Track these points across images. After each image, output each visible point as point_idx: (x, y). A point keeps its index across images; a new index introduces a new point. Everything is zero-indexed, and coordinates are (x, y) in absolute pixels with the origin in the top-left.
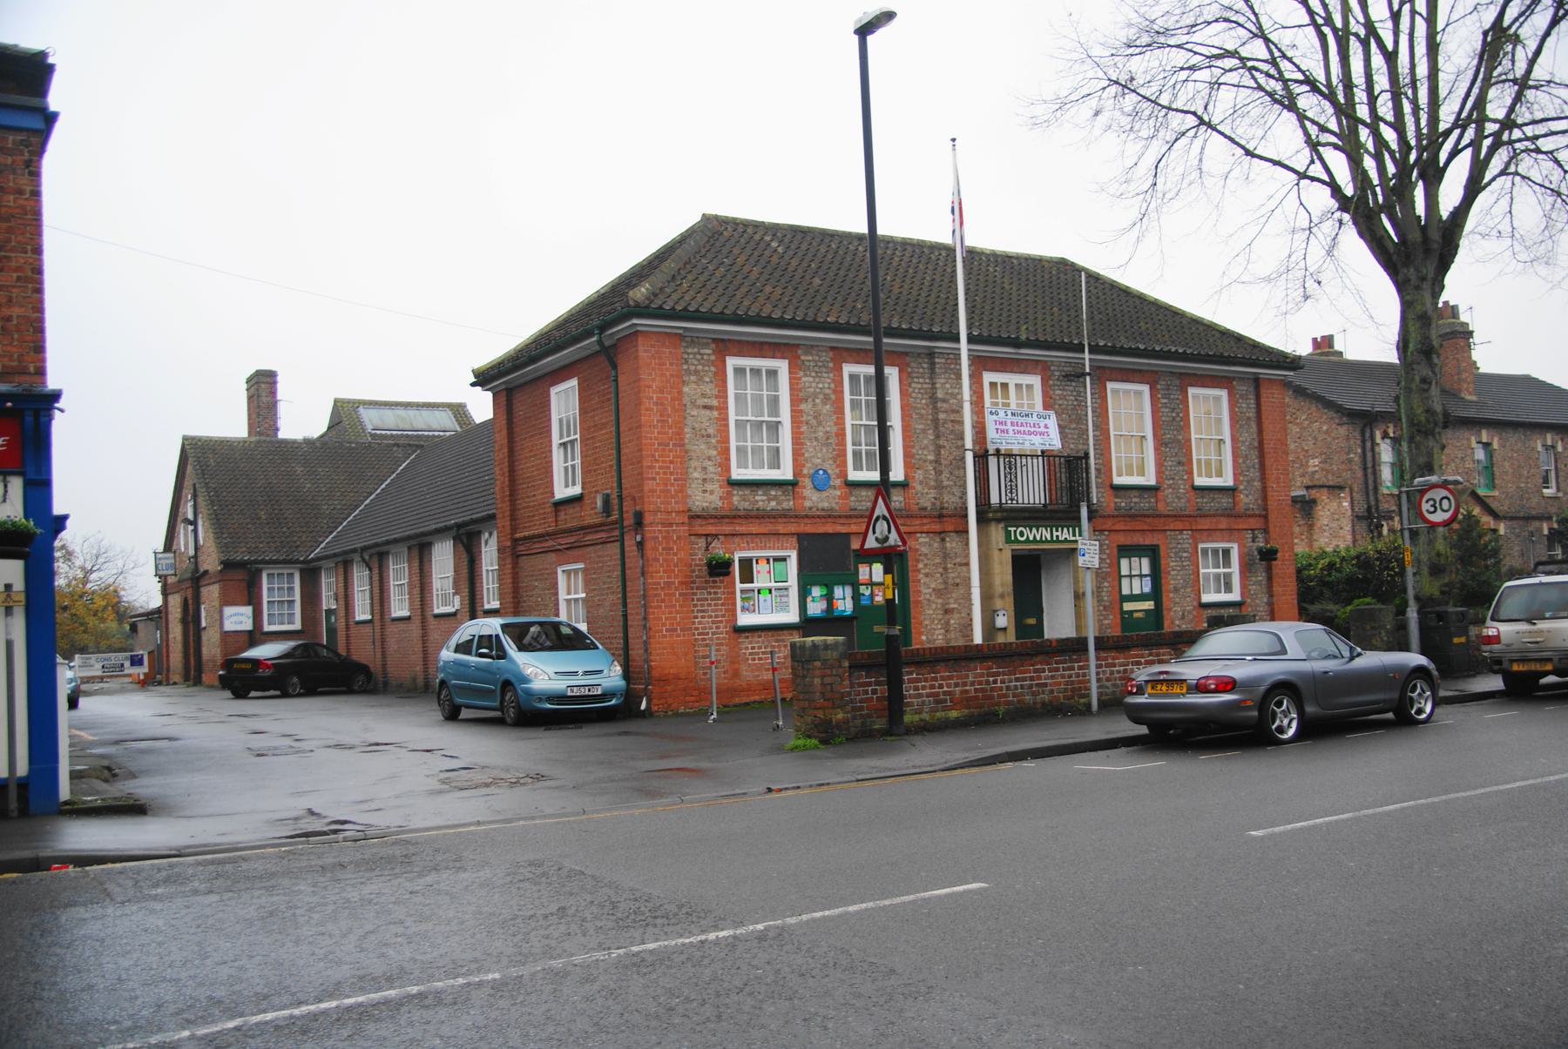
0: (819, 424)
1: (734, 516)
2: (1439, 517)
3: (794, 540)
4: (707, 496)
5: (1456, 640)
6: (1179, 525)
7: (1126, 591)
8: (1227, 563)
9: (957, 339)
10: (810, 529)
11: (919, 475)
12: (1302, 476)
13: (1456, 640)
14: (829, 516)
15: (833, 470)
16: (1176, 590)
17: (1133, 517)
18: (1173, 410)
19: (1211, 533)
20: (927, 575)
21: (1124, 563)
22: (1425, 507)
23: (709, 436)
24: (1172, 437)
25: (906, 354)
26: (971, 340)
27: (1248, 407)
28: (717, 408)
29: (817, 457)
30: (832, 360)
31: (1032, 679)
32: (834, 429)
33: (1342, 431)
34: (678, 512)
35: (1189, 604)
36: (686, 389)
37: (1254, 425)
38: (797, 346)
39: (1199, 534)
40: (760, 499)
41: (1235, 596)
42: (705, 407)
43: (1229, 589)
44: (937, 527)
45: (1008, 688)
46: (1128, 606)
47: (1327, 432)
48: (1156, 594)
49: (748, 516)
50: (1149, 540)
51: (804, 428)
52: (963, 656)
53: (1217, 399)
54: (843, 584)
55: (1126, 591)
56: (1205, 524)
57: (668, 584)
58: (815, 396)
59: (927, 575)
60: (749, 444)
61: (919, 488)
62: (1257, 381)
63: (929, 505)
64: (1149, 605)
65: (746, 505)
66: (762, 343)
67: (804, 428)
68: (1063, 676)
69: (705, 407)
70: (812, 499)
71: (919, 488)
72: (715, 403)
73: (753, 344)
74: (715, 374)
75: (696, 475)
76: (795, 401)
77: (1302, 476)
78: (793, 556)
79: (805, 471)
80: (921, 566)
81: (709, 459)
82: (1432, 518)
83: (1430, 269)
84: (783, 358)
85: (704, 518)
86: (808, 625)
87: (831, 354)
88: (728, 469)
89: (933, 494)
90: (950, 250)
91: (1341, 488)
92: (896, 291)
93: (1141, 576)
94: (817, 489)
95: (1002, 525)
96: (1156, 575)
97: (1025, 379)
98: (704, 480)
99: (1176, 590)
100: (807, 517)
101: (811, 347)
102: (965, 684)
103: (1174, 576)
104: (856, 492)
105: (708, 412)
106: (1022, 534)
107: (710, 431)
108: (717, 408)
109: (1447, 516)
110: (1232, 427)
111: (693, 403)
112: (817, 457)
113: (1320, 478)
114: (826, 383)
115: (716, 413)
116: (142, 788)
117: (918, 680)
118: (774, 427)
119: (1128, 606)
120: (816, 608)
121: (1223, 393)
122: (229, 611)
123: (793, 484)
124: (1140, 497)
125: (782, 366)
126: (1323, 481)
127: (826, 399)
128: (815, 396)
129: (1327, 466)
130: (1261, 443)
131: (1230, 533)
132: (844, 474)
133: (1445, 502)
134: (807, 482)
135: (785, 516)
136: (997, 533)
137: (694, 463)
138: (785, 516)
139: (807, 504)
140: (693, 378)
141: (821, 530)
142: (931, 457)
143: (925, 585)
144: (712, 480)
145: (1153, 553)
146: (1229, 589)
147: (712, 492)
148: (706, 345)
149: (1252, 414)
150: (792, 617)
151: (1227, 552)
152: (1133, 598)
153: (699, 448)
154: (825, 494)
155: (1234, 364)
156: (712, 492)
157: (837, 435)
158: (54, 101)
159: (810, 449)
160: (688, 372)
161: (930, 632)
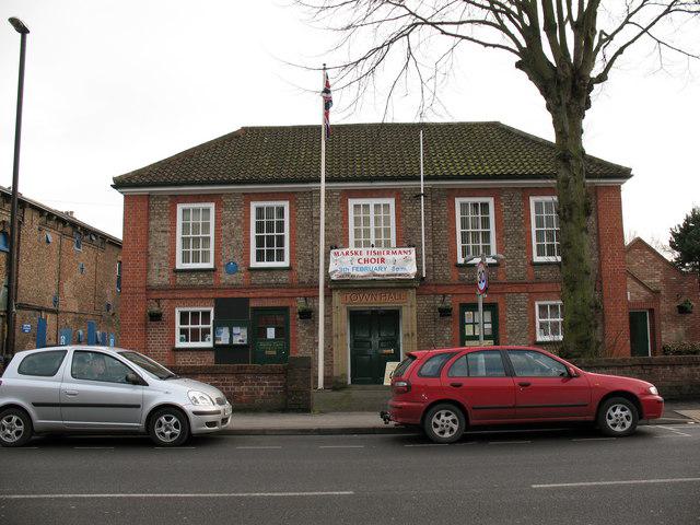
0: (233, 236)
1: (176, 288)
4: (159, 278)
6: (516, 289)
10: (222, 295)
11: (300, 263)
14: (234, 288)
16: (512, 333)
18: (515, 213)
26: (328, 180)
29: (230, 254)
36: (152, 223)
39: (534, 295)
40: (193, 279)
54: (241, 326)
56: (538, 288)
58: (230, 221)
76: (217, 225)
84: (389, 197)
86: (217, 348)
94: (229, 272)
96: (495, 321)
99: (512, 333)
101: (229, 195)
105: (163, 234)
107: (165, 244)
114: (239, 214)
116: (396, 410)
118: (486, 236)
122: (269, 337)
123: (214, 270)
125: (212, 206)
128: (230, 221)
136: (336, 297)
138: (205, 288)
141: (230, 296)
150: (208, 344)
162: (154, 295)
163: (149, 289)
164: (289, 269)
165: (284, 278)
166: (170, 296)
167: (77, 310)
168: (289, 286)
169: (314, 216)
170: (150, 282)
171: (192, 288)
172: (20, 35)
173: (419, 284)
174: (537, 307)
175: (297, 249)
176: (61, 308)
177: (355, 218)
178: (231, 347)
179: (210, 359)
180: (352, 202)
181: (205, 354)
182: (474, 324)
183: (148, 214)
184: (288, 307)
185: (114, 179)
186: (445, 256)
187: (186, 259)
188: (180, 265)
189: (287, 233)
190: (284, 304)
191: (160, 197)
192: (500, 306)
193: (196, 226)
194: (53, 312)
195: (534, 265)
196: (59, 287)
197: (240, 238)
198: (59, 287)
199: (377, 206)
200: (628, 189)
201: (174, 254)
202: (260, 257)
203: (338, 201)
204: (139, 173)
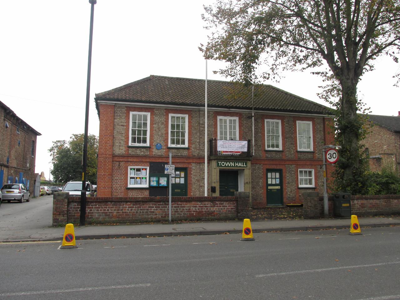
1: (129, 156)
2: (332, 160)
3: (149, 163)
5: (344, 205)
7: (269, 182)
8: (310, 175)
9: (205, 106)
11: (193, 146)
12: (382, 151)
13: (344, 205)
15: (163, 144)
16: (288, 183)
17: (273, 160)
18: (290, 128)
19: (303, 166)
20: (194, 175)
21: (269, 175)
22: (328, 156)
23: (122, 133)
24: (290, 136)
25: (191, 111)
26: (208, 106)
27: (320, 127)
28: (126, 126)
29: (158, 140)
30: (165, 112)
31: (148, 210)
32: (165, 132)
33: (393, 137)
34: (109, 155)
35: (294, 188)
36: (116, 120)
37: (323, 133)
38: (154, 109)
39: (298, 166)
40: (138, 152)
41: (313, 186)
42: (122, 125)
43: (311, 183)
44: (199, 161)
45: (137, 212)
46: (270, 188)
47: (389, 138)
48: (281, 184)
49: (133, 156)
50: (278, 167)
51: (154, 132)
52: (201, 199)
53: (277, 123)
55: (269, 182)
57: (104, 175)
58: (159, 122)
59: (194, 175)
60: (175, 138)
61: (193, 149)
62: (324, 119)
63: (196, 155)
64: (278, 187)
65: (133, 153)
66: (142, 108)
67: (154, 132)
68: (161, 210)
69: (122, 125)
70: (155, 152)
71: (193, 149)
72: (125, 124)
73: (139, 108)
74: (126, 116)
75: (117, 144)
77: (382, 151)
78: (148, 168)
79: (154, 144)
80: (192, 172)
81: (122, 140)
82: (330, 160)
83: (352, 75)
85: (118, 156)
86: (151, 188)
87: (165, 111)
88: (128, 143)
89: (198, 151)
90: (204, 81)
91: (392, 154)
92: (284, 103)
93: (276, 178)
95: (216, 161)
96: (281, 178)
97: (233, 118)
98: (120, 146)
99: (288, 183)
100: (153, 157)
101: (158, 109)
102: (118, 210)
103: (288, 177)
104: (171, 150)
105: (122, 127)
106: (223, 164)
107: (123, 132)
108: (126, 126)
109: (335, 160)
110: (313, 133)
111: (118, 124)
112: (158, 140)
113: (387, 152)
114: (163, 119)
115: (125, 127)
117: (99, 208)
119: (270, 188)
120: (154, 184)
121: (311, 123)
123: (149, 148)
124: (301, 155)
126: (388, 152)
127: (162, 124)
128: (159, 122)
129: (389, 148)
130: (325, 138)
131: (311, 166)
132: (167, 145)
133: (334, 155)
134: (154, 147)
135: (145, 157)
137: (117, 141)
138: (145, 157)
139: (154, 153)
140: (118, 117)
142: (198, 141)
143: (193, 178)
144: (122, 146)
145: (280, 171)
146: (311, 183)
147: (122, 149)
148: (124, 108)
149: (322, 129)
150: (147, 186)
151: (310, 172)
152: (272, 185)
153: (118, 136)
154: (159, 151)
155: (313, 113)
156: (122, 149)
157: (165, 134)
158: (149, 76)
159: (156, 137)
160: (117, 116)
161: (194, 192)
162: (116, 159)
163: (114, 156)
164: (188, 149)
165: (185, 153)
166: (125, 160)
167: (16, 166)
168: (188, 158)
169: (201, 122)
170: (114, 152)
171: (138, 156)
172: (90, 5)
173: (244, 157)
174: (299, 171)
175: (192, 139)
176: (10, 165)
177: (146, 120)
178: (179, 184)
179: (146, 194)
180: (219, 118)
181: (144, 191)
182: (272, 178)
183: (114, 116)
184: (187, 168)
185: (96, 95)
186: (260, 146)
187: (173, 142)
188: (130, 144)
189: (170, 130)
190: (185, 166)
191: (120, 107)
192: (284, 171)
193: (178, 126)
194: (7, 167)
195: (297, 152)
196: (10, 152)
197: (163, 131)
198: (10, 152)
199: (230, 121)
200: (97, 93)
201: (128, 138)
202: (134, 140)
203: (213, 116)
204: (109, 93)
